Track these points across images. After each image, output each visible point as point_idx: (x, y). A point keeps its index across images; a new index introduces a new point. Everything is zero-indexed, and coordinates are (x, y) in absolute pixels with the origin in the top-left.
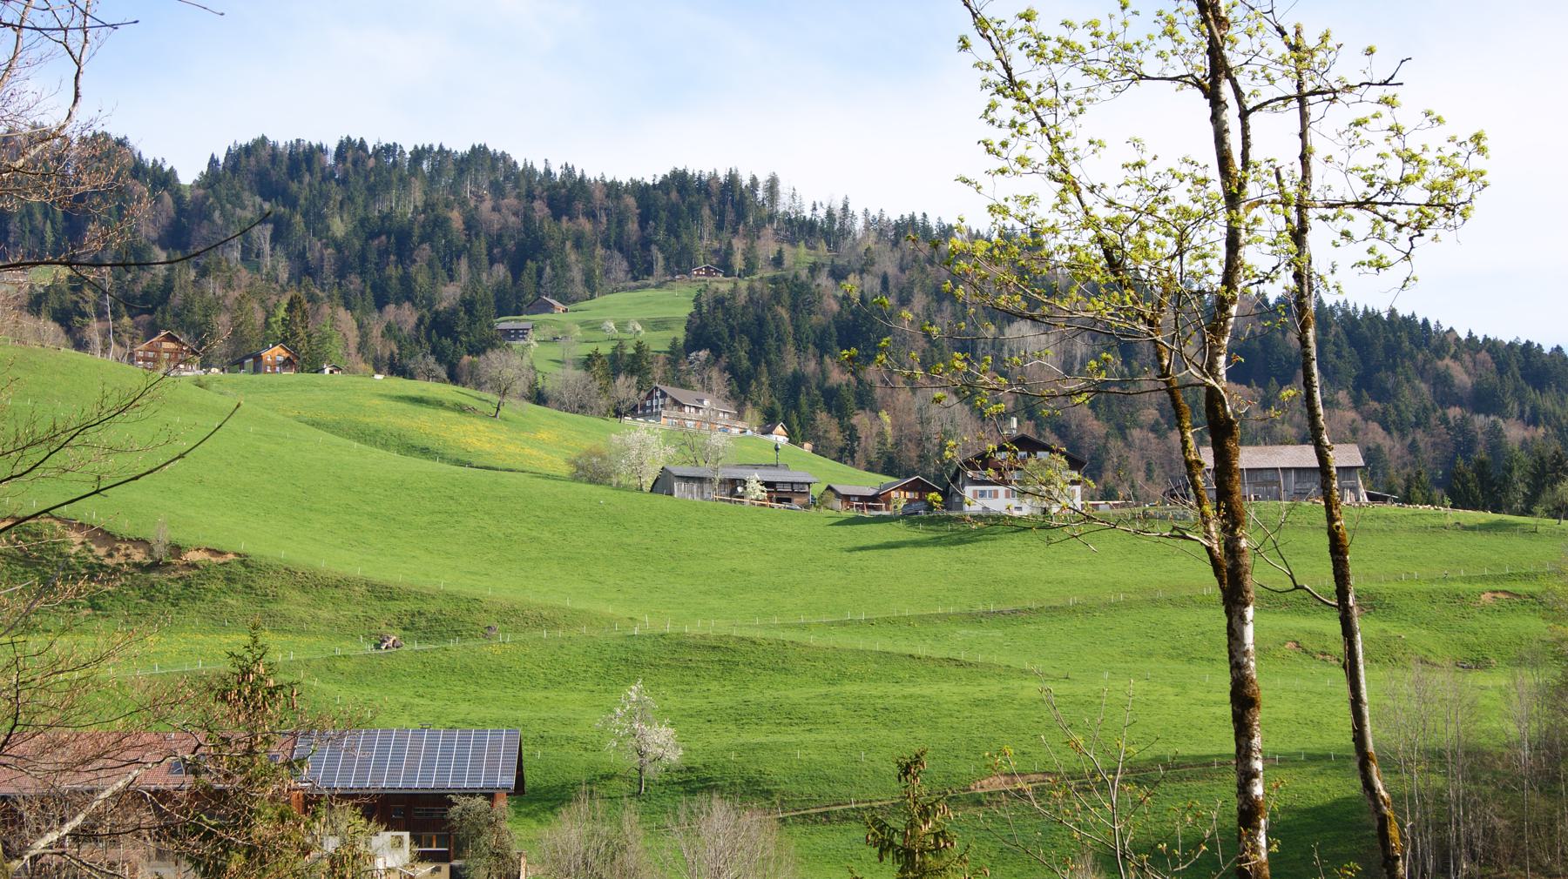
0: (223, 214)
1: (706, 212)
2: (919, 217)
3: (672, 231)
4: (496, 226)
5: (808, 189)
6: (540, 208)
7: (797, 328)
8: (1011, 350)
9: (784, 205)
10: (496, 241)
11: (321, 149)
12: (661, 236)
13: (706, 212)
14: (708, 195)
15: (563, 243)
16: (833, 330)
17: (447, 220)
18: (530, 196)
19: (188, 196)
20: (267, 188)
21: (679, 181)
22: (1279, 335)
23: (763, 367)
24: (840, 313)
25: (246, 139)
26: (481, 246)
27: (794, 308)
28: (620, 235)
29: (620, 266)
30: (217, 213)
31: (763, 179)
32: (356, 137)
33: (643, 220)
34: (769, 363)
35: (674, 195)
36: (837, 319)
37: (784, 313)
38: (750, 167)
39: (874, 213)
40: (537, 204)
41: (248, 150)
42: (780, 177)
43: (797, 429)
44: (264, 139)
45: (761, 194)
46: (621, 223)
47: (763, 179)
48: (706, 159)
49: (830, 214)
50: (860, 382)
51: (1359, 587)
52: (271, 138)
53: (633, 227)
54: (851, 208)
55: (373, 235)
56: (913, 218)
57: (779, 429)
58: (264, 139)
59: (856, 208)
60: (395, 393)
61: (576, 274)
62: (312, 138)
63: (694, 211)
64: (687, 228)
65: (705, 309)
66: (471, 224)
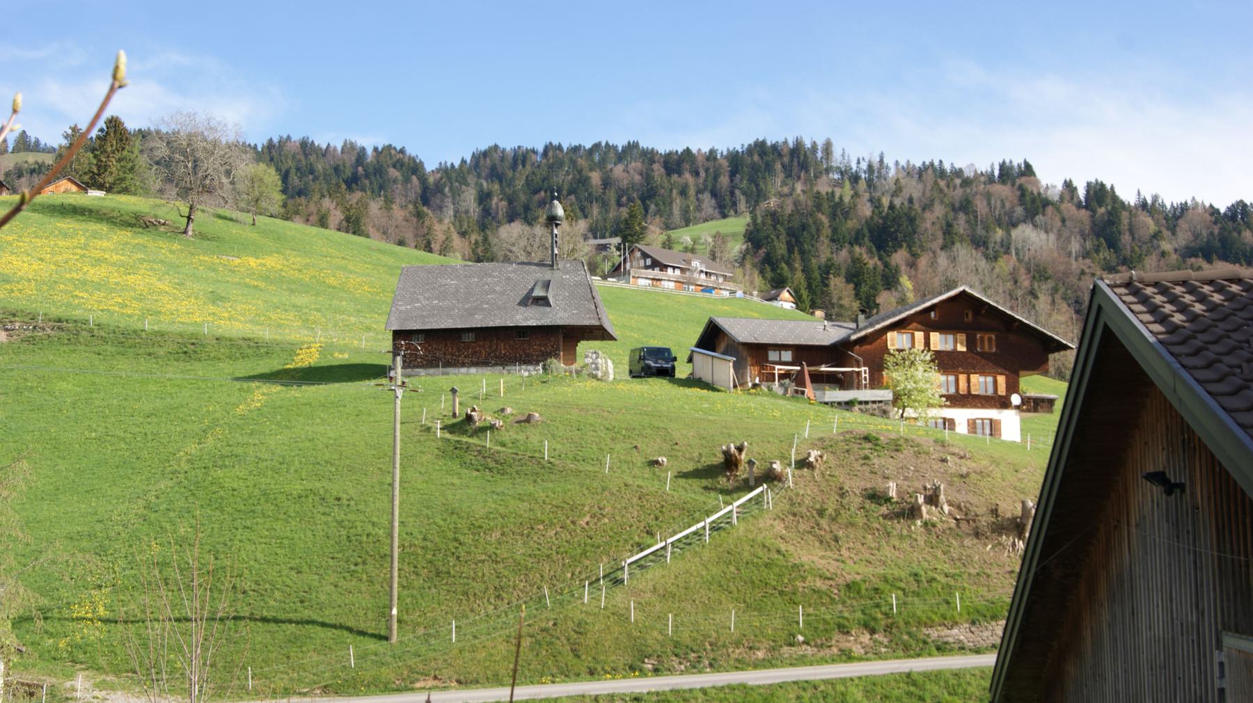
0: (451, 189)
1: (778, 166)
2: (936, 163)
3: (752, 180)
4: (625, 182)
5: (854, 150)
6: (658, 169)
7: (835, 231)
8: (1017, 249)
9: (837, 159)
10: (621, 193)
11: (534, 151)
12: (745, 184)
13: (778, 166)
14: (780, 155)
15: (671, 191)
16: (866, 231)
17: (588, 178)
18: (652, 161)
19: (431, 180)
20: (495, 174)
21: (760, 147)
22: (1235, 234)
23: (797, 255)
24: (872, 218)
25: (483, 147)
26: (612, 196)
27: (833, 216)
28: (714, 187)
29: (708, 202)
30: (447, 189)
31: (820, 143)
32: (555, 143)
33: (733, 174)
34: (802, 252)
35: (756, 158)
36: (868, 222)
37: (824, 219)
38: (811, 134)
39: (903, 163)
40: (656, 166)
41: (485, 154)
42: (834, 141)
43: (805, 293)
44: (496, 147)
45: (819, 155)
46: (716, 178)
47: (820, 143)
48: (777, 133)
49: (870, 167)
50: (886, 265)
51: (1048, 416)
52: (502, 146)
53: (724, 180)
54: (886, 161)
55: (536, 192)
56: (932, 164)
57: (785, 294)
58: (496, 147)
59: (889, 161)
60: (238, 225)
61: (676, 210)
62: (527, 145)
63: (769, 168)
64: (764, 178)
65: (759, 220)
66: (606, 183)
